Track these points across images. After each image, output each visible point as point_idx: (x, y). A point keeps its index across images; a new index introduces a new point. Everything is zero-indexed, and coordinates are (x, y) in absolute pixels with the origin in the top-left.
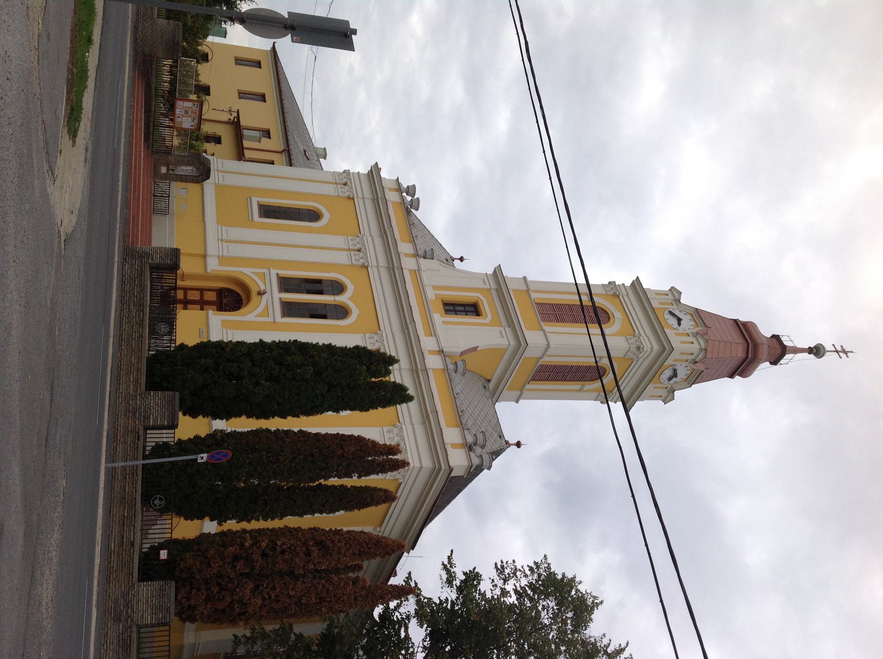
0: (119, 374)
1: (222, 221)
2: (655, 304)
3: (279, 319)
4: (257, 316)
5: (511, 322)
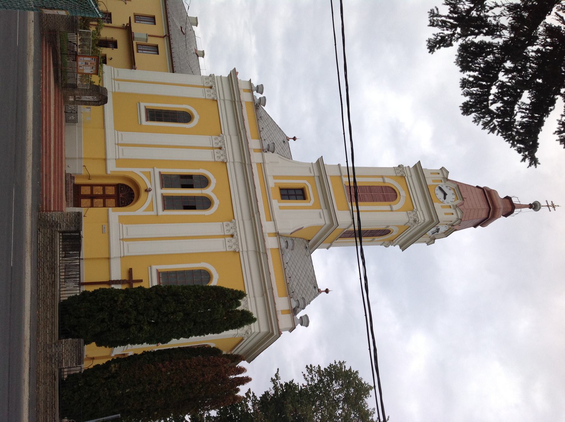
0: (38, 327)
1: (118, 127)
2: (429, 182)
3: (161, 212)
4: (144, 211)
5: (328, 206)
